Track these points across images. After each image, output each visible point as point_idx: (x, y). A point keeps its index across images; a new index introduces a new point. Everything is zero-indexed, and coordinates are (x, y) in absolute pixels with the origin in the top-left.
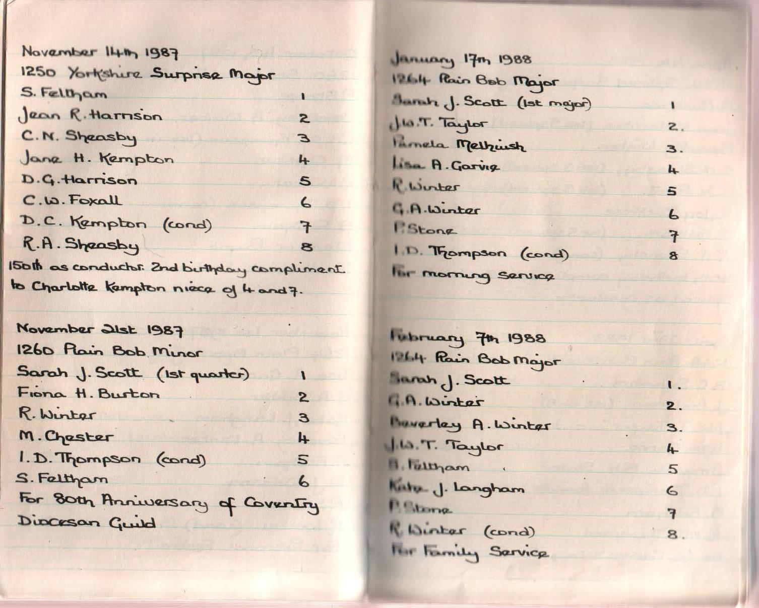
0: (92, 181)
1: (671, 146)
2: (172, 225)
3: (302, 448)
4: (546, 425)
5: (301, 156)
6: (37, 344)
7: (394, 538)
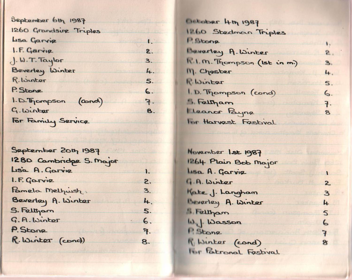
3: (146, 206)
4: (266, 52)
7: (190, 246)
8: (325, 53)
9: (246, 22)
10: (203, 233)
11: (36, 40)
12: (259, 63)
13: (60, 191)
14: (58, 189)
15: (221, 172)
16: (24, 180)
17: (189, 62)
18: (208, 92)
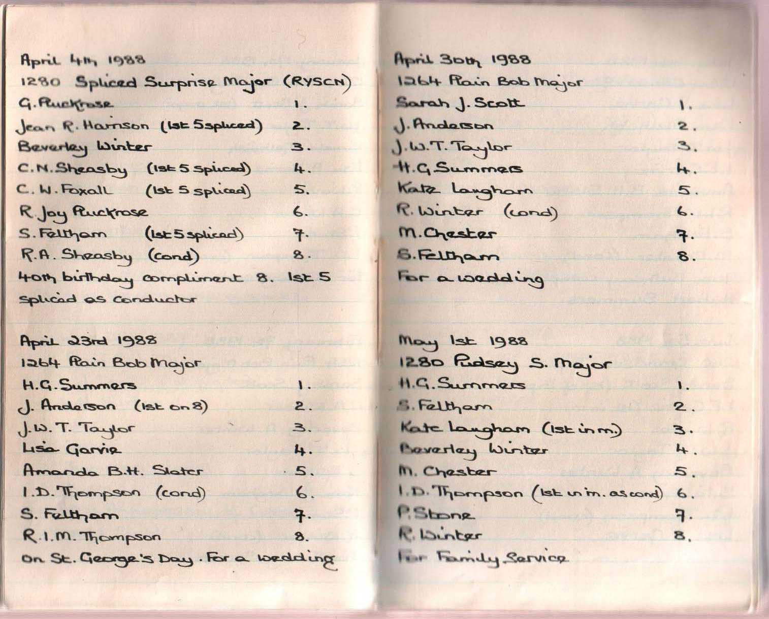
1: (682, 142)
2: (166, 494)
8: (679, 126)
9: (499, 340)
10: (431, 517)
12: (138, 407)
14: (439, 403)
17: (403, 536)
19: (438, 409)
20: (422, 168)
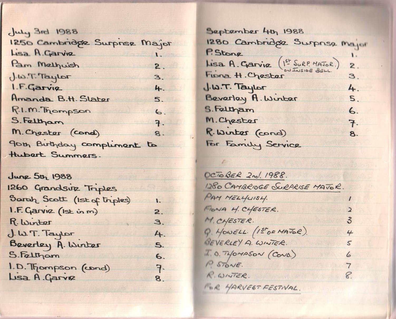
0: (52, 44)
5: (156, 86)
6: (18, 185)
11: (40, 187)
13: (55, 65)
15: (31, 87)
16: (23, 210)
18: (46, 110)
19: (225, 122)
20: (244, 64)
